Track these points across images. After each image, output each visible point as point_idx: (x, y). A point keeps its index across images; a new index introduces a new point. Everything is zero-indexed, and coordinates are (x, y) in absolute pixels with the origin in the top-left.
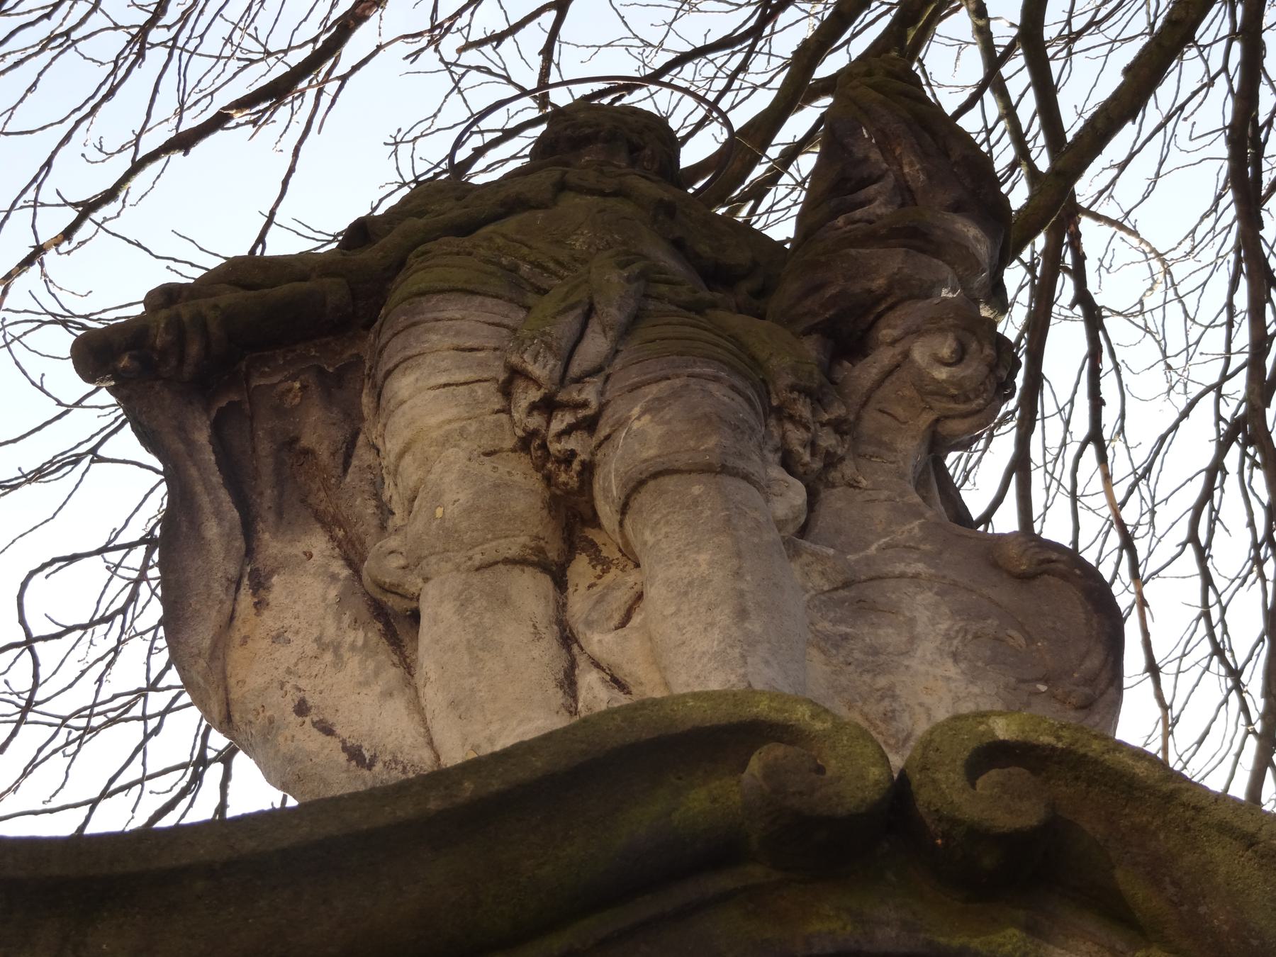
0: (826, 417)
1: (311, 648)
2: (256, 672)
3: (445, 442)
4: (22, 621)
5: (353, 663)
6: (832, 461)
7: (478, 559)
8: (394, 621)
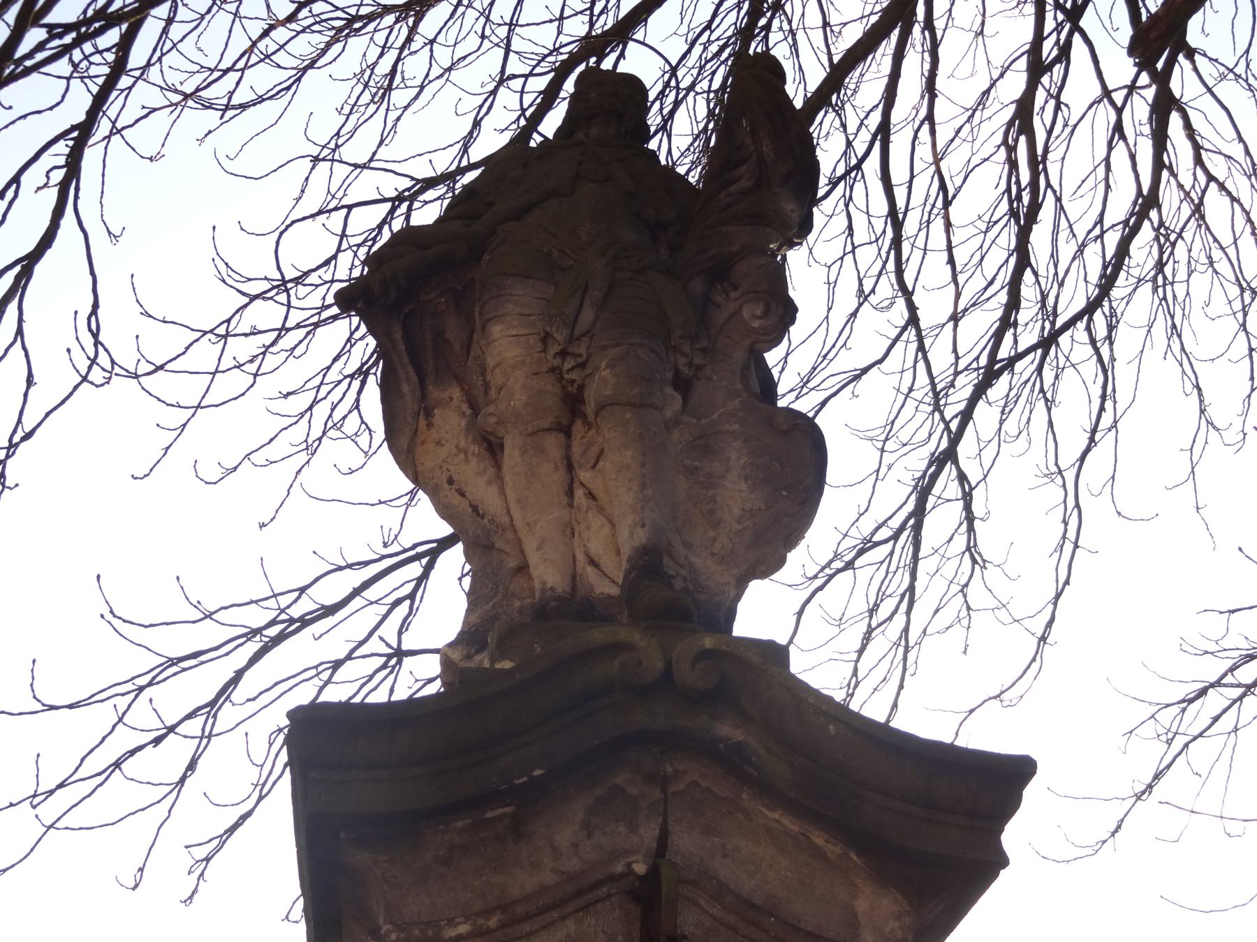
0: (698, 346)
1: (454, 450)
2: (429, 458)
3: (515, 367)
4: (279, 268)
5: (474, 461)
6: (699, 368)
7: (530, 430)
8: (493, 448)
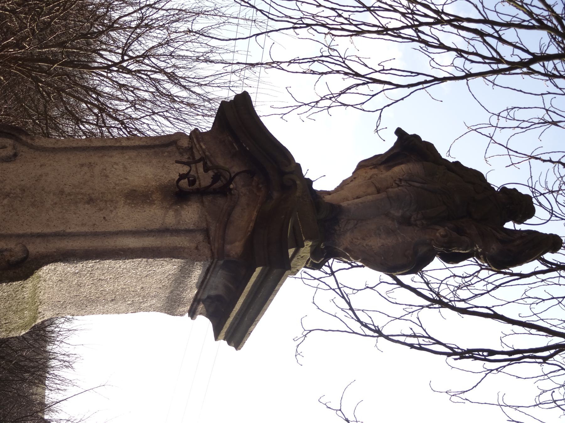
6: (416, 225)
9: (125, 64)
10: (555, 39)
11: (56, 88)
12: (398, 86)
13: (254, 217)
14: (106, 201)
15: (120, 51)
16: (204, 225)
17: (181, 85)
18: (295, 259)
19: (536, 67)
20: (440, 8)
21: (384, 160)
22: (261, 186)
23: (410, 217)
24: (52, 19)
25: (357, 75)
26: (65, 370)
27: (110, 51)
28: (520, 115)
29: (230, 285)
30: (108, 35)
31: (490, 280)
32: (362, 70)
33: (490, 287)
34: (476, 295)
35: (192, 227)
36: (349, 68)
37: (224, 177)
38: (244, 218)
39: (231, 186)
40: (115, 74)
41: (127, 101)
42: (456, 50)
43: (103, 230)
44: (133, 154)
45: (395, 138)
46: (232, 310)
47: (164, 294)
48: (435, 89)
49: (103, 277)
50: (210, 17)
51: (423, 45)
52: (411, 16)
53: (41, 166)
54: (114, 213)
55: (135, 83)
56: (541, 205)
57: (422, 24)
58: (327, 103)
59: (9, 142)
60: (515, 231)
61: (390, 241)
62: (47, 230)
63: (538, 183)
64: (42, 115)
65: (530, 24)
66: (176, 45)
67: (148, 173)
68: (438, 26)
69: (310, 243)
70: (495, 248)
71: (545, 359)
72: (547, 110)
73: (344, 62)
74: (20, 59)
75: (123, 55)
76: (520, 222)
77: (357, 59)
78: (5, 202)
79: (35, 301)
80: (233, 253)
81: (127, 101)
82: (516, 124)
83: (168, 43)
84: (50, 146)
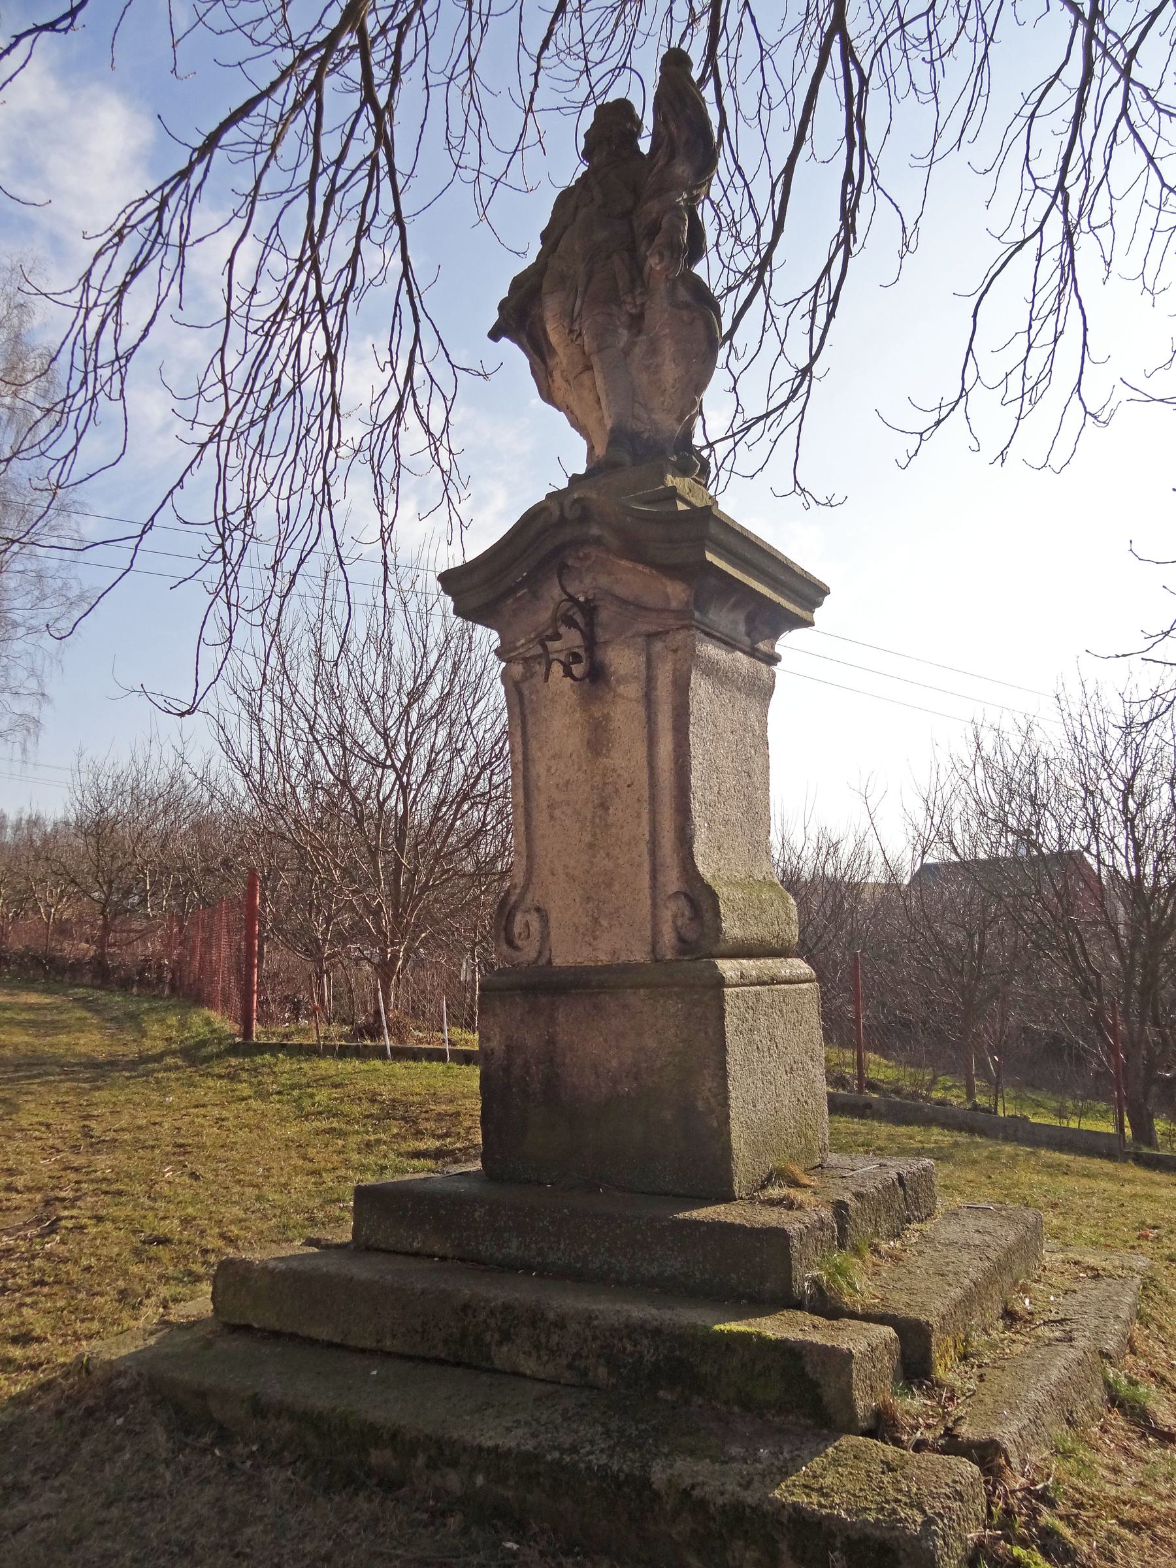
6: (643, 305)
9: (398, 765)
10: (336, 65)
11: (436, 861)
12: (417, 339)
13: (629, 564)
14: (605, 784)
15: (379, 771)
16: (639, 640)
17: (425, 684)
18: (693, 500)
19: (382, 97)
20: (293, 265)
21: (538, 360)
22: (581, 554)
23: (631, 315)
24: (336, 866)
25: (399, 408)
26: (840, 853)
27: (380, 784)
28: (457, 129)
29: (732, 600)
30: (356, 789)
31: (726, 180)
32: (392, 400)
33: (738, 180)
34: (751, 206)
35: (643, 659)
36: (390, 418)
37: (568, 610)
38: (631, 579)
39: (582, 599)
40: (413, 778)
41: (452, 759)
42: (358, 238)
43: (647, 787)
44: (534, 745)
45: (505, 341)
46: (771, 598)
47: (742, 701)
48: (421, 276)
49: (716, 789)
50: (324, 640)
51: (351, 297)
52: (306, 316)
53: (553, 874)
54: (622, 772)
55: (424, 750)
56: (605, 92)
57: (318, 296)
58: (443, 453)
59: (519, 919)
60: (655, 135)
61: (668, 348)
62: (647, 867)
63: (567, 95)
64: (474, 882)
65: (314, 107)
66: (367, 689)
67: (562, 725)
68: (322, 267)
69: (669, 477)
70: (682, 168)
71: (864, 81)
72: (451, 79)
73: (381, 426)
74: (396, 909)
75: (384, 766)
76: (639, 124)
77: (375, 406)
78: (605, 923)
79: (747, 884)
80: (683, 596)
81: (452, 759)
82: (471, 139)
83: (364, 702)
84: (524, 862)
